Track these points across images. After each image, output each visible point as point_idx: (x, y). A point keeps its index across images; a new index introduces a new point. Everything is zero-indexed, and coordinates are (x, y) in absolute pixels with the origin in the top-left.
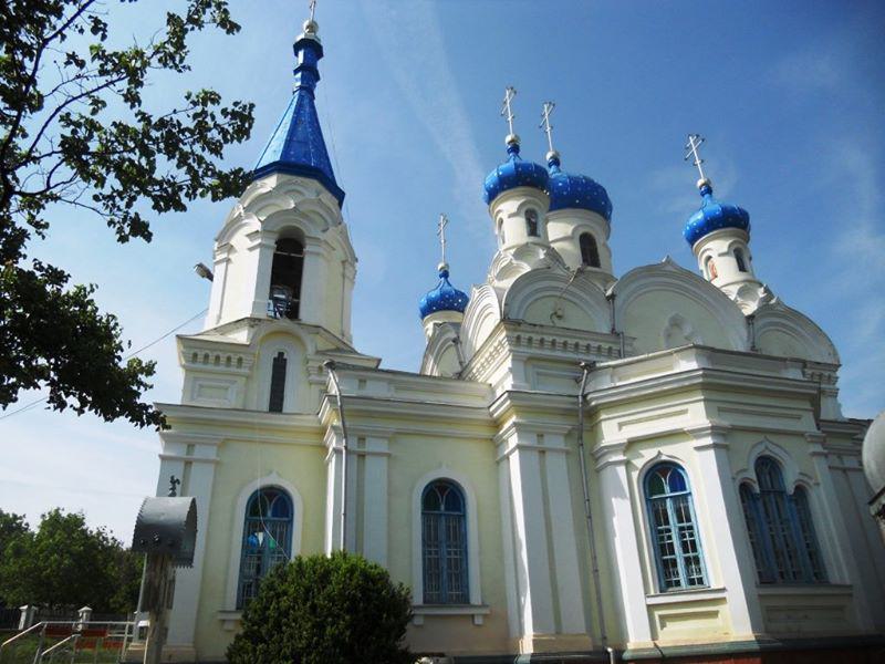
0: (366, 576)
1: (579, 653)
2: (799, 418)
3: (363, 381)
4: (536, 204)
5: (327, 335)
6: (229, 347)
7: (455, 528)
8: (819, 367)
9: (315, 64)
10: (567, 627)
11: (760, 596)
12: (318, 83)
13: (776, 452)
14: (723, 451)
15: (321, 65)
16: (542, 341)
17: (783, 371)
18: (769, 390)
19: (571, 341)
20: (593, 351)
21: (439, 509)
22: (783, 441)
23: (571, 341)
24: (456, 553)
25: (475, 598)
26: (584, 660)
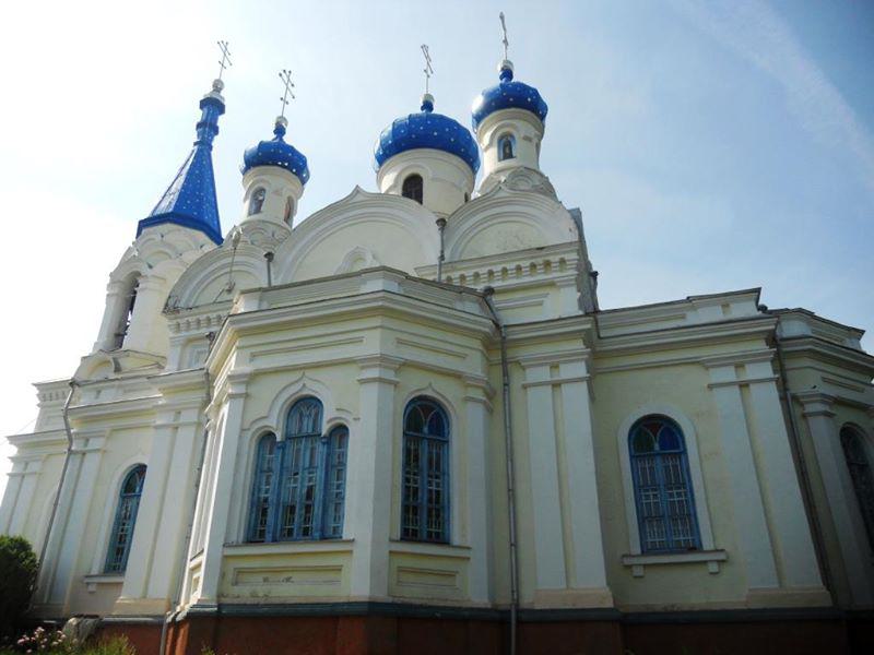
0: (16, 541)
1: (148, 616)
2: (361, 341)
3: (726, 306)
4: (508, 126)
5: (137, 355)
6: (57, 385)
7: (675, 467)
8: (543, 252)
9: (216, 120)
10: (152, 593)
11: (391, 552)
12: (216, 138)
13: (313, 389)
14: (390, 390)
15: (222, 121)
16: (199, 322)
17: (362, 286)
18: (334, 315)
19: (511, 266)
20: (214, 322)
21: (652, 448)
22: (321, 374)
23: (511, 266)
24: (679, 495)
25: (707, 544)
26: (151, 622)
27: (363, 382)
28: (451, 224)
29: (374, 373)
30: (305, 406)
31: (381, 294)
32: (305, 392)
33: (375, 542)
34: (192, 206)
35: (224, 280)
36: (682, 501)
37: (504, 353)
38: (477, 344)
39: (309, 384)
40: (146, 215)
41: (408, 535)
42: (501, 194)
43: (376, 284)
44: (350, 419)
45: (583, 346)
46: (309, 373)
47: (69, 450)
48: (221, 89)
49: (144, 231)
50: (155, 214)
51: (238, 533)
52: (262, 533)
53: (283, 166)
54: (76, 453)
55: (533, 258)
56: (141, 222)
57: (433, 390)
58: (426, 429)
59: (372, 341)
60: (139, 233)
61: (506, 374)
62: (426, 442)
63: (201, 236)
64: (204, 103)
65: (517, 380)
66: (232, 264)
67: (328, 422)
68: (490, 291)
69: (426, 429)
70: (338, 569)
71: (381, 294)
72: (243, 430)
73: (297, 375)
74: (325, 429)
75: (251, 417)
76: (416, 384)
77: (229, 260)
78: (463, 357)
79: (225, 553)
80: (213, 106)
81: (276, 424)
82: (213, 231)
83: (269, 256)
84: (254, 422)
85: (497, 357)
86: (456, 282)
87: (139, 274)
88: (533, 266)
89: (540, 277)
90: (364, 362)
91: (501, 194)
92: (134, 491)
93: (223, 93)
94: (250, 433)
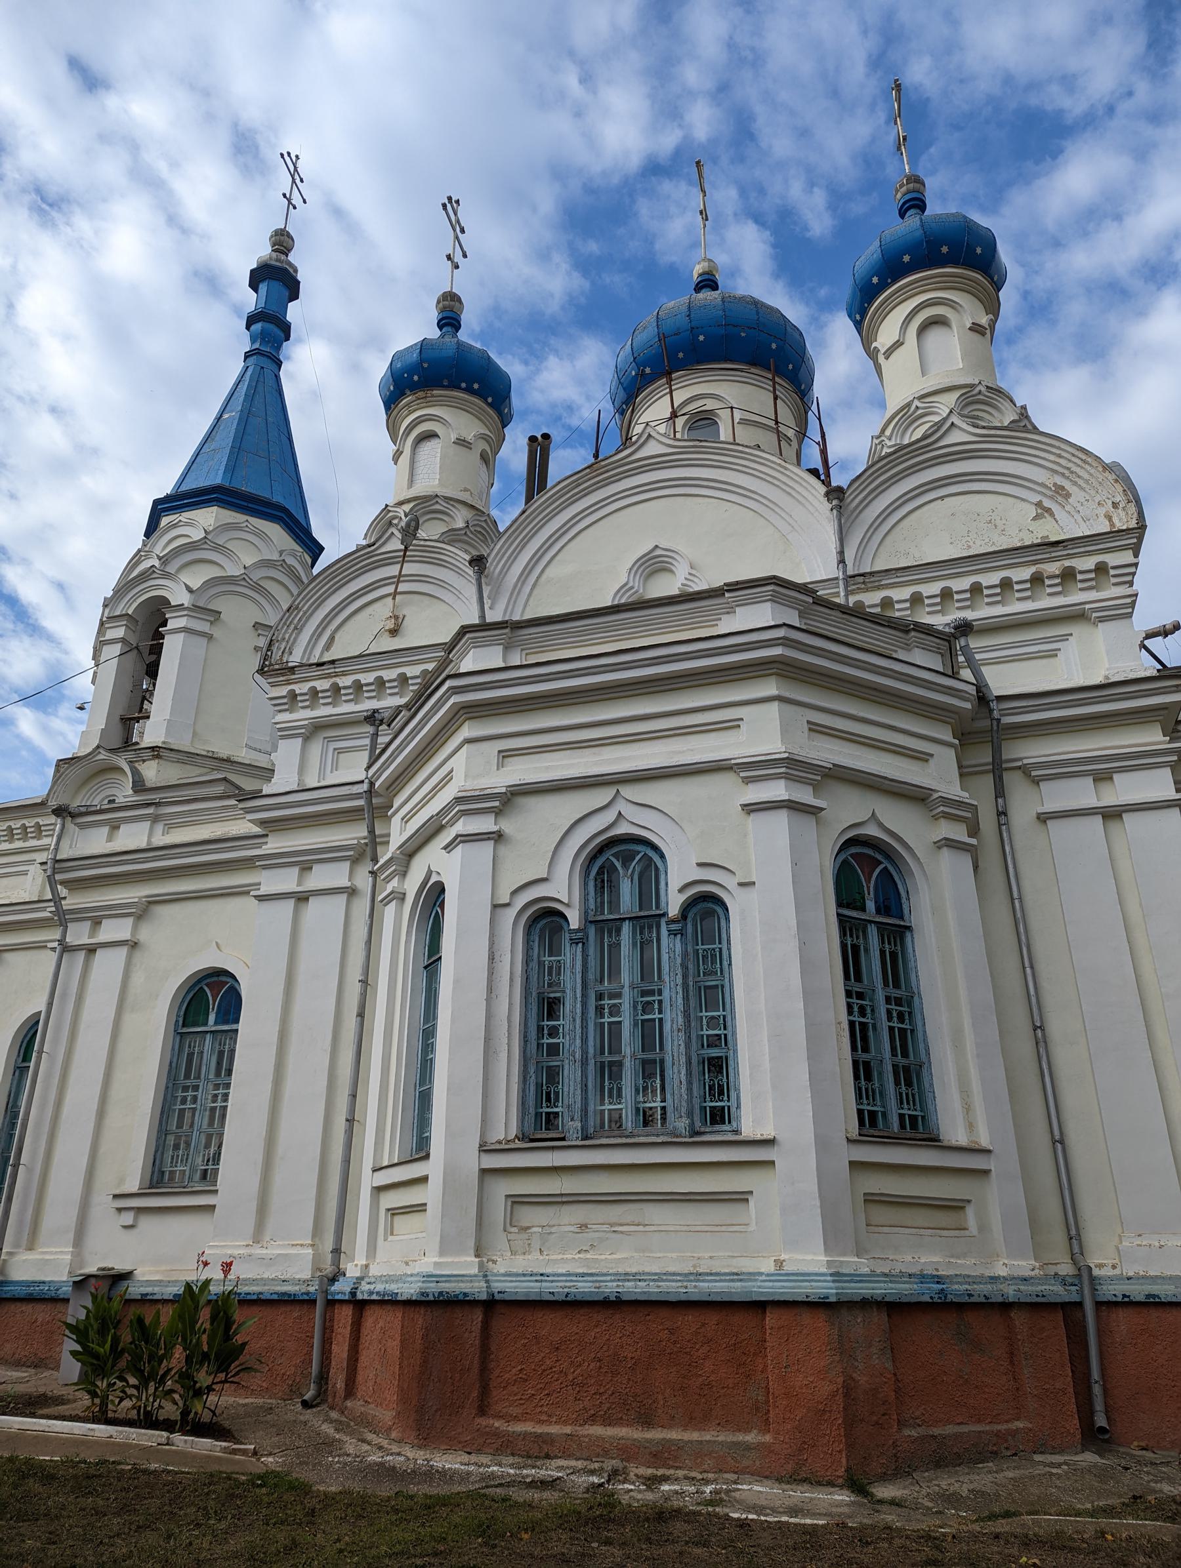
11: (852, 1164)
13: (636, 822)
14: (809, 823)
19: (1023, 574)
27: (751, 809)
28: (852, 500)
29: (778, 790)
30: (618, 859)
31: (781, 633)
32: (622, 829)
33: (822, 1144)
34: (247, 471)
35: (383, 610)
36: (905, 1030)
37: (997, 752)
38: (946, 735)
39: (629, 811)
40: (166, 487)
41: (870, 1123)
42: (955, 437)
43: (758, 615)
44: (730, 882)
45: (1161, 738)
46: (628, 791)
47: (61, 942)
48: (290, 250)
49: (165, 521)
50: (184, 488)
51: (505, 1126)
52: (551, 1120)
53: (469, 390)
54: (78, 948)
55: (1035, 562)
56: (156, 503)
57: (881, 825)
58: (871, 905)
59: (763, 727)
60: (152, 528)
61: (1000, 792)
62: (872, 931)
63: (275, 532)
64: (258, 277)
65: (1025, 804)
66: (399, 578)
67: (680, 891)
68: (965, 628)
69: (871, 905)
70: (956, 1207)
71: (781, 633)
72: (495, 906)
73: (602, 796)
74: (674, 904)
75: (511, 880)
76: (850, 811)
77: (393, 570)
78: (922, 758)
79: (484, 1166)
80: (277, 278)
81: (564, 888)
82: (297, 522)
83: (478, 562)
84: (515, 892)
85: (984, 756)
86: (900, 612)
87: (164, 601)
88: (1037, 580)
89: (1045, 602)
90: (752, 770)
91: (955, 437)
92: (206, 1024)
93: (292, 258)
94: (512, 913)
